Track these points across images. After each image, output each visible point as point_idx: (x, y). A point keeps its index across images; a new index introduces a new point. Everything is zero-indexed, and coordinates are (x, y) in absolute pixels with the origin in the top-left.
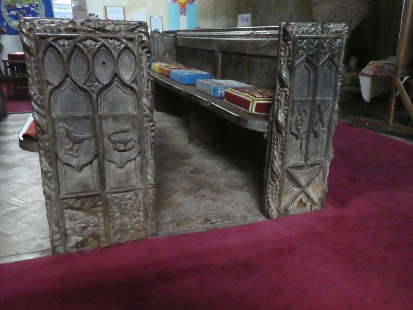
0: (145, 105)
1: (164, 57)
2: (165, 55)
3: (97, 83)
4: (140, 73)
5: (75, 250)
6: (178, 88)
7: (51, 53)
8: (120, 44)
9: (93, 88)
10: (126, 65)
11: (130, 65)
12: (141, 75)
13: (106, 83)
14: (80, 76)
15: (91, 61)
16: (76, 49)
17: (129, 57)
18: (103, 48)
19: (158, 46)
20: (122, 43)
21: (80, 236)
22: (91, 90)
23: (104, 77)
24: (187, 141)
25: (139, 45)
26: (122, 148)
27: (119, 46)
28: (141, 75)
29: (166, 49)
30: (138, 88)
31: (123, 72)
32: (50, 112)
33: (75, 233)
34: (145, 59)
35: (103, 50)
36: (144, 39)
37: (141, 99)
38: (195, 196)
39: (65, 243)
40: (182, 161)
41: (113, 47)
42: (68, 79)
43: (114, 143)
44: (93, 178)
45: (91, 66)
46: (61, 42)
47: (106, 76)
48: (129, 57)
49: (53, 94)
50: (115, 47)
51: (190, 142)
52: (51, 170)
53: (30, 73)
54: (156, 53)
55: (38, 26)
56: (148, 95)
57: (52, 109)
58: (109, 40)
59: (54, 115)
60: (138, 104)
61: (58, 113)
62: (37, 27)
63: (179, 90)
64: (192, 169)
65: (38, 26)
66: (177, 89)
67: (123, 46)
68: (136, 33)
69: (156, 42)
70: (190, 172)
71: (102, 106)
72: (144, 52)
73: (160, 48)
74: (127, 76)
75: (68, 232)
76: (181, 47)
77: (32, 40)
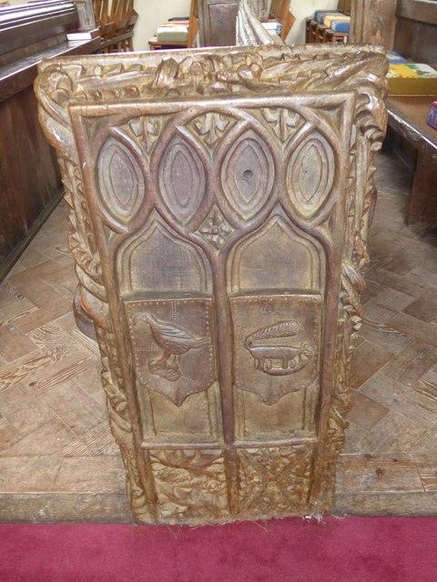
0: (347, 277)
1: (372, 38)
2: (374, 34)
3: (226, 227)
4: (345, 199)
5: (173, 522)
6: (399, 120)
7: (116, 152)
8: (298, 123)
9: (215, 238)
10: (308, 176)
11: (318, 173)
12: (348, 202)
13: (249, 224)
14: (185, 206)
15: (213, 174)
16: (177, 140)
17: (318, 153)
18: (250, 134)
19: (363, 17)
20: (304, 118)
21: (182, 505)
22: (211, 242)
23: (245, 208)
24: (400, 219)
25: (354, 121)
26: (277, 368)
27: (293, 127)
28: (348, 202)
29: (379, 21)
30: (333, 239)
31: (299, 194)
32: (117, 285)
33: (172, 498)
34: (365, 158)
35: (248, 139)
36: (370, 106)
37: (339, 263)
38: (417, 388)
39: (154, 513)
40: (390, 274)
41: (277, 131)
42: (155, 216)
43: (259, 358)
44: (208, 414)
45: (213, 186)
46: (136, 126)
47: (251, 206)
48: (318, 153)
49: (122, 250)
50: (282, 131)
51: (407, 222)
52: (123, 396)
53: (70, 202)
54: (358, 31)
55: (79, 85)
56: (356, 257)
57: (120, 279)
58: (267, 110)
59: (125, 292)
60: (328, 277)
61: (136, 288)
62: (76, 87)
63: (401, 125)
64: (410, 300)
65: (79, 85)
66: (397, 121)
67: (307, 127)
68: (350, 89)
69: (360, 9)
70: (406, 311)
71: (236, 276)
72: (363, 140)
73: (366, 19)
74: (308, 202)
75: (161, 496)
76: (408, 19)
77: (67, 124)
